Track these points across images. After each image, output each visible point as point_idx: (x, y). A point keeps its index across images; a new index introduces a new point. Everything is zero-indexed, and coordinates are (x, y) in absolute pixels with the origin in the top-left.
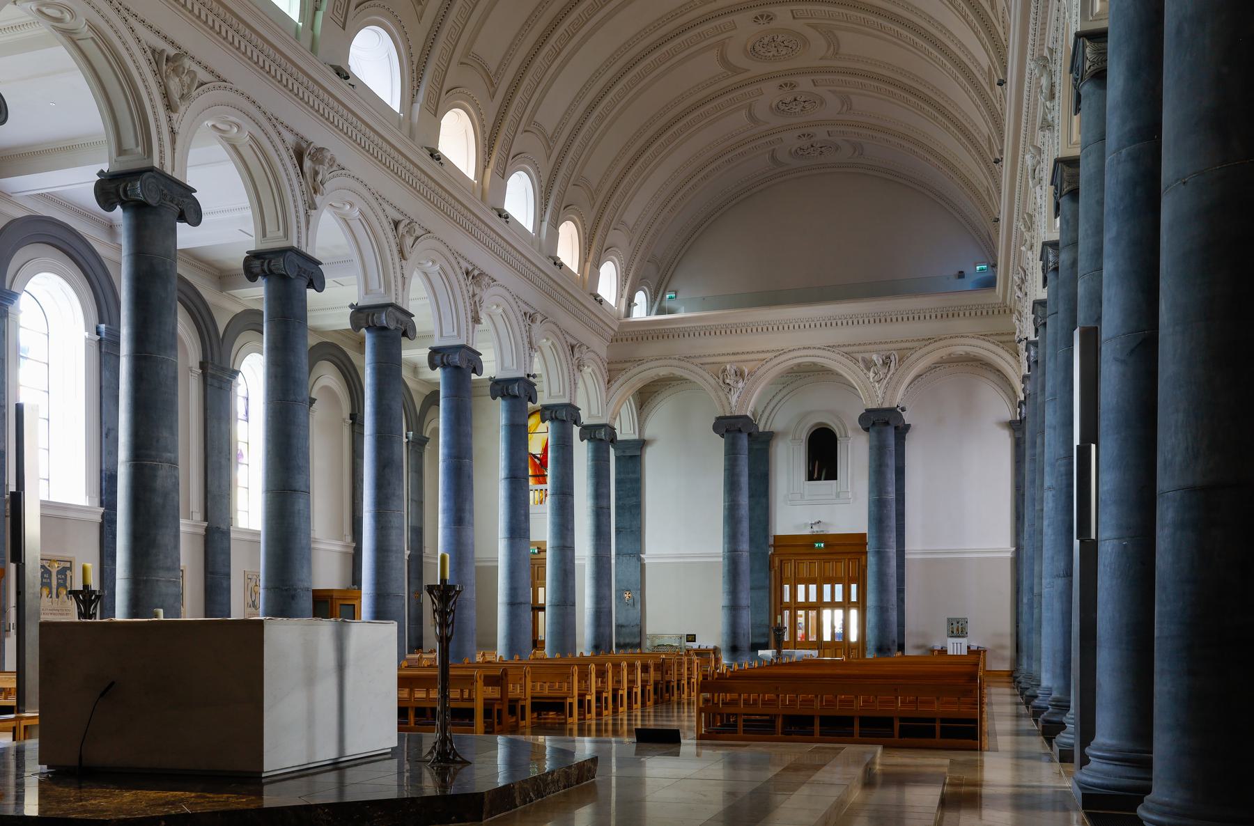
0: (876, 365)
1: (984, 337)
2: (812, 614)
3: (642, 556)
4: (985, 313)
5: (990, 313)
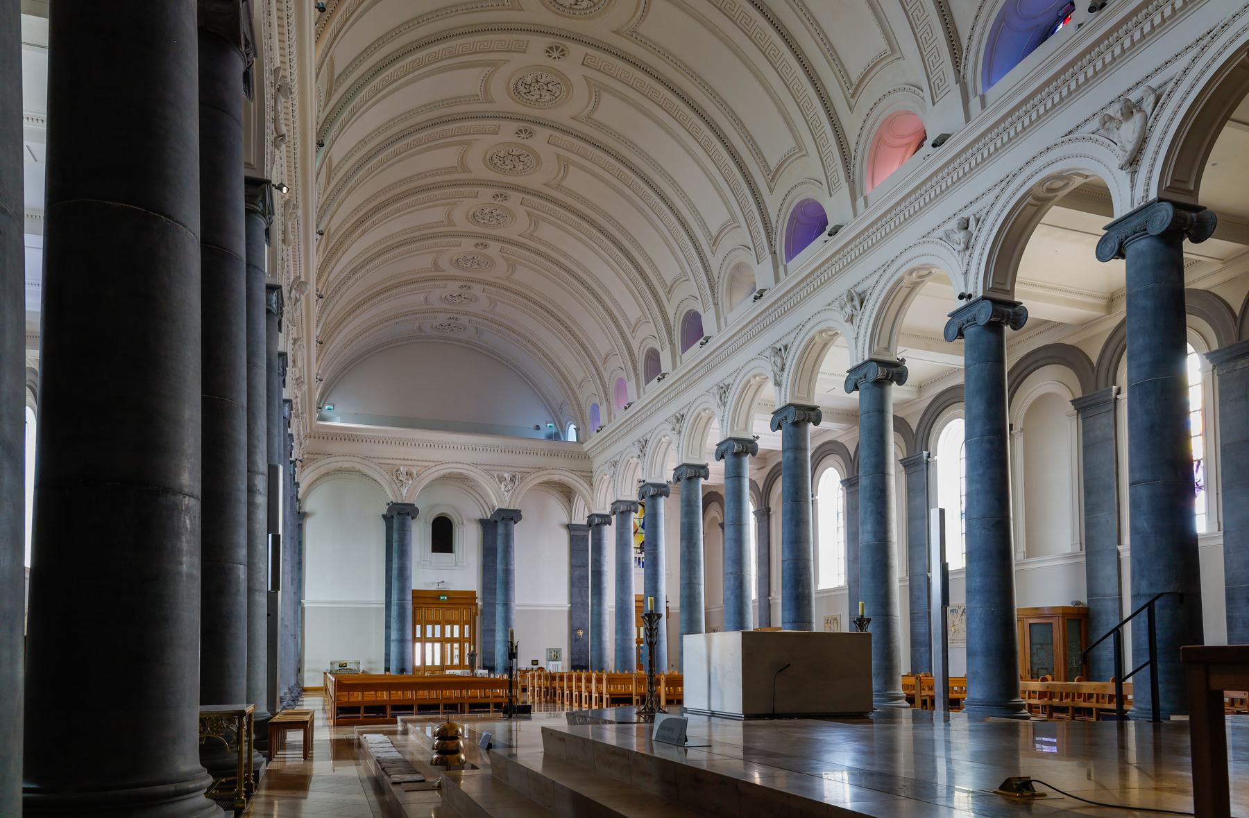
0: (506, 480)
1: (572, 471)
2: (456, 645)
3: (303, 601)
4: (573, 457)
5: (577, 457)
